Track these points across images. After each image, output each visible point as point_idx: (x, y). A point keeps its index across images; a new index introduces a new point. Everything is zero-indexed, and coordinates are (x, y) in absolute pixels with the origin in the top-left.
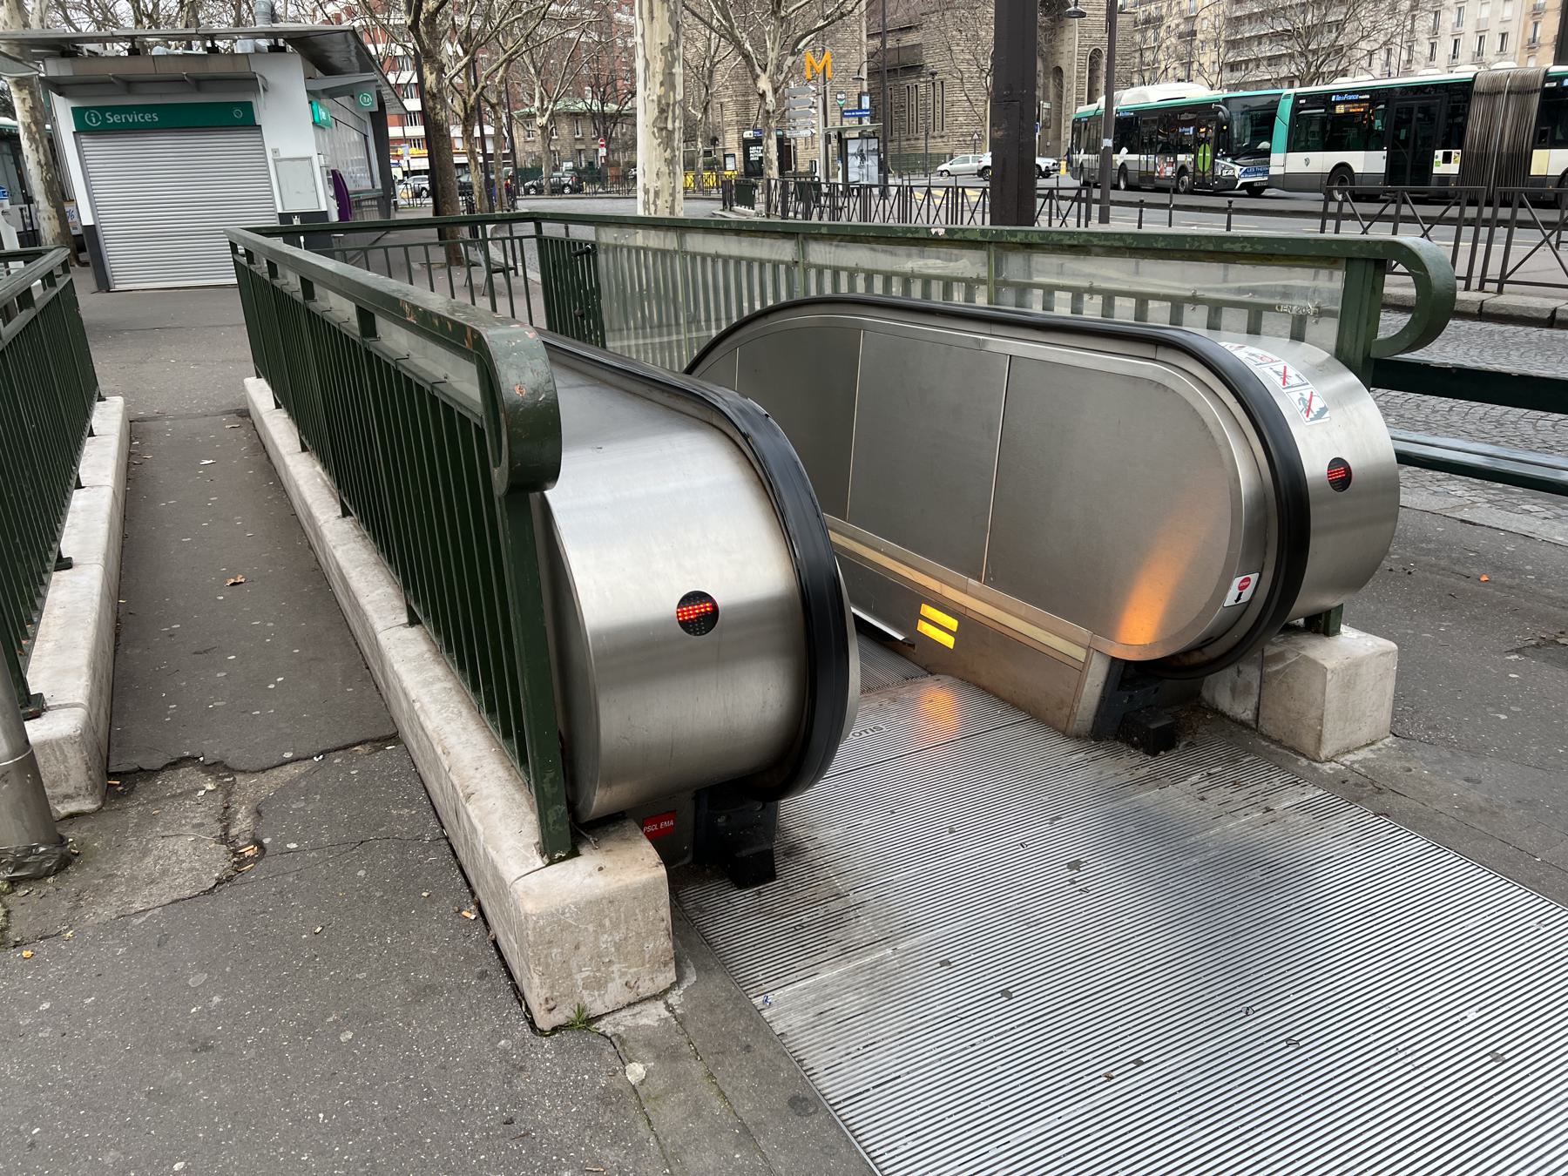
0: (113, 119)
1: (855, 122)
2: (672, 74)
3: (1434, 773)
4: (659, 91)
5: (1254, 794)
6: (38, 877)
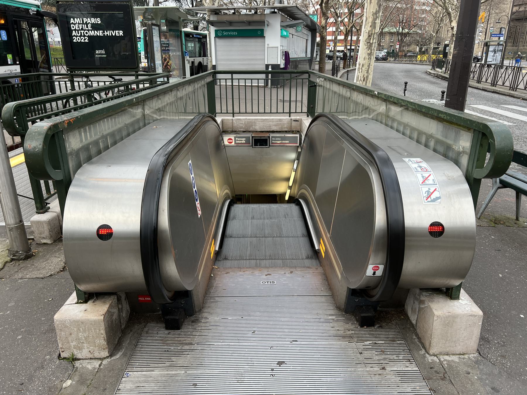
0: (225, 33)
1: (497, 39)
2: (375, 23)
3: (480, 379)
4: (369, 29)
5: (385, 359)
6: (19, 260)
